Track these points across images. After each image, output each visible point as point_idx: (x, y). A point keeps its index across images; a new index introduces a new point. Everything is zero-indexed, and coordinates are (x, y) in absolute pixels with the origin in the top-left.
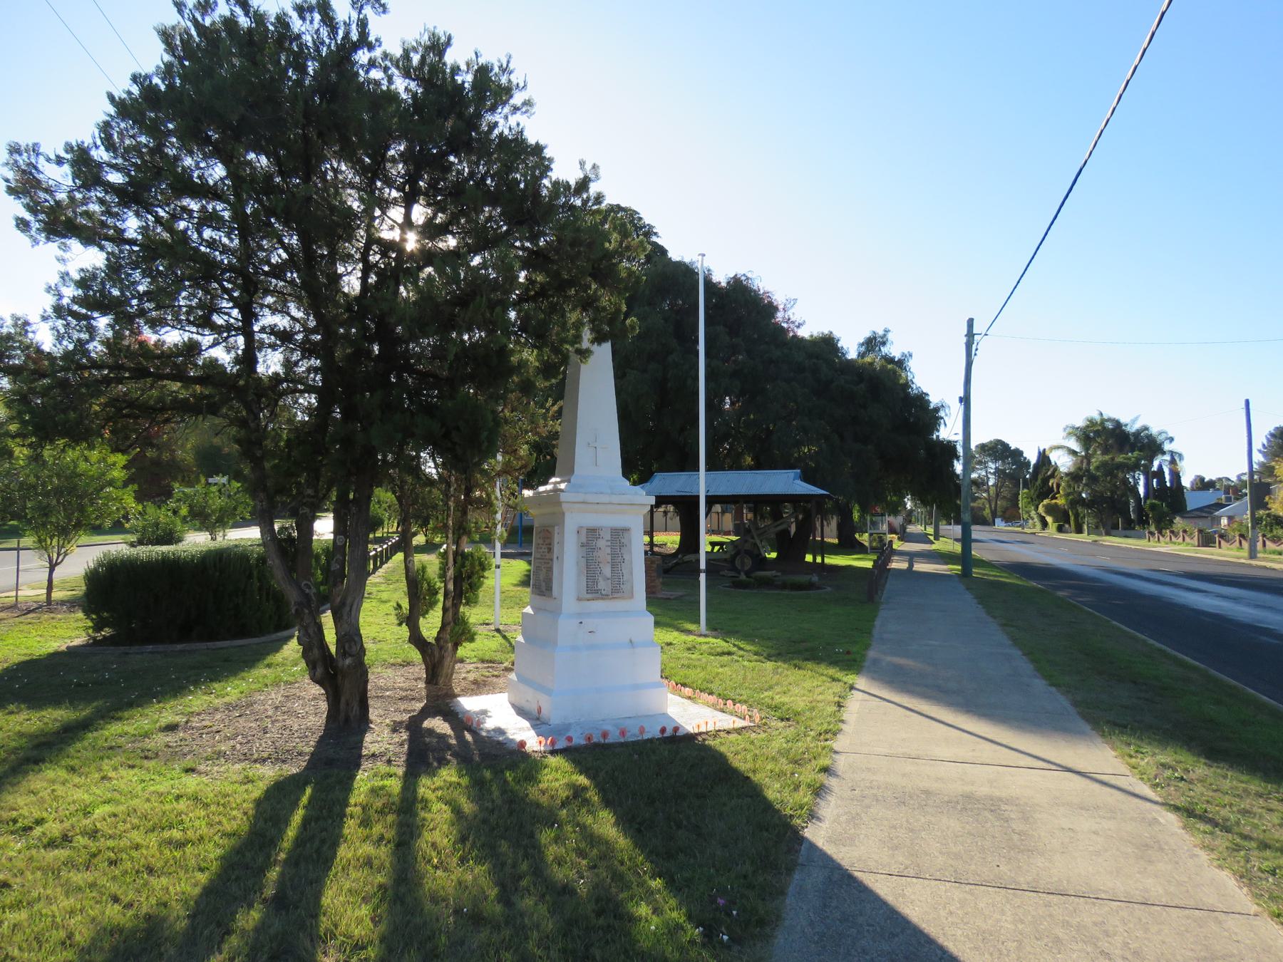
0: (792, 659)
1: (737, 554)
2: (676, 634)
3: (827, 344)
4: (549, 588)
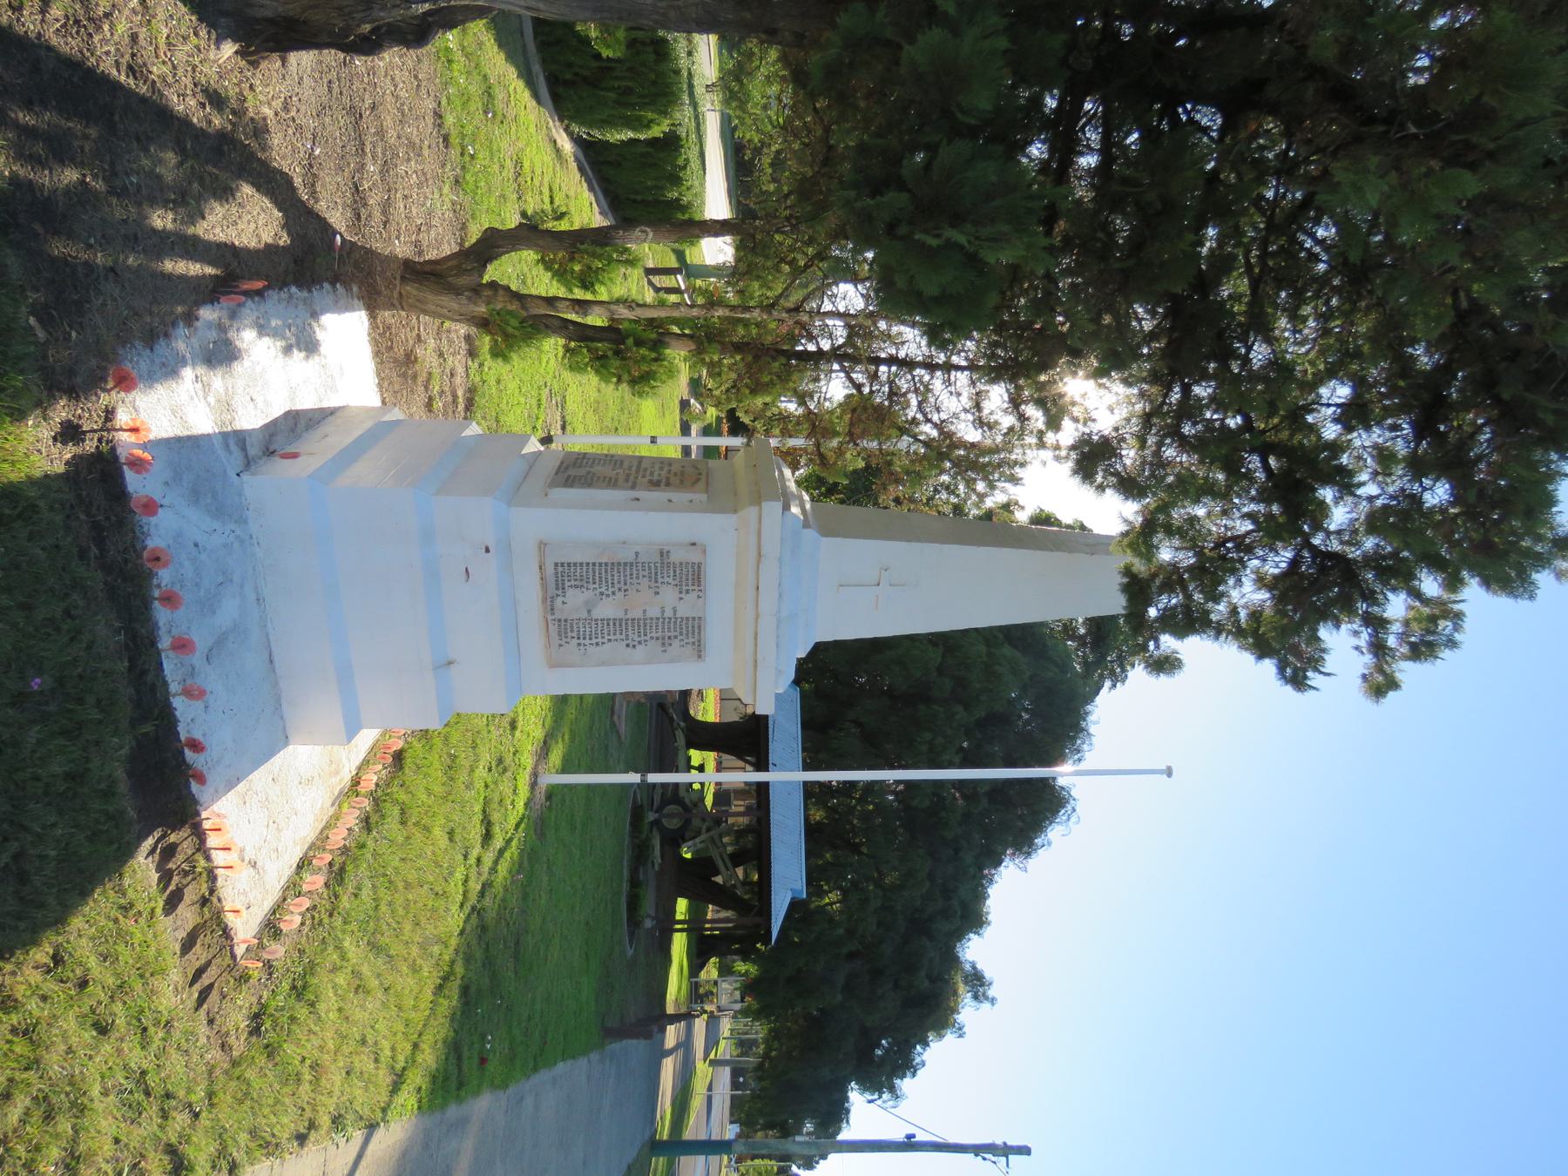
0: (468, 960)
1: (686, 809)
2: (539, 733)
3: (973, 919)
4: (569, 482)
